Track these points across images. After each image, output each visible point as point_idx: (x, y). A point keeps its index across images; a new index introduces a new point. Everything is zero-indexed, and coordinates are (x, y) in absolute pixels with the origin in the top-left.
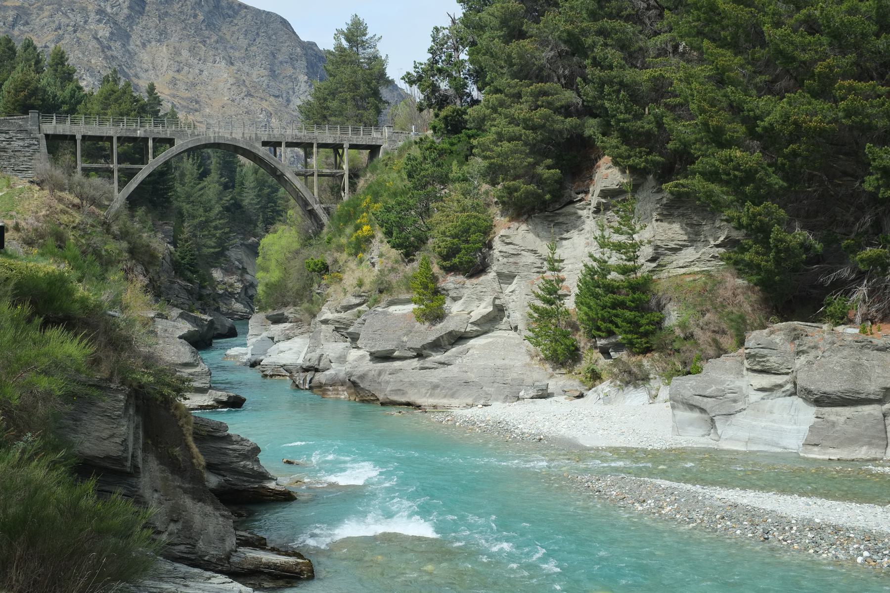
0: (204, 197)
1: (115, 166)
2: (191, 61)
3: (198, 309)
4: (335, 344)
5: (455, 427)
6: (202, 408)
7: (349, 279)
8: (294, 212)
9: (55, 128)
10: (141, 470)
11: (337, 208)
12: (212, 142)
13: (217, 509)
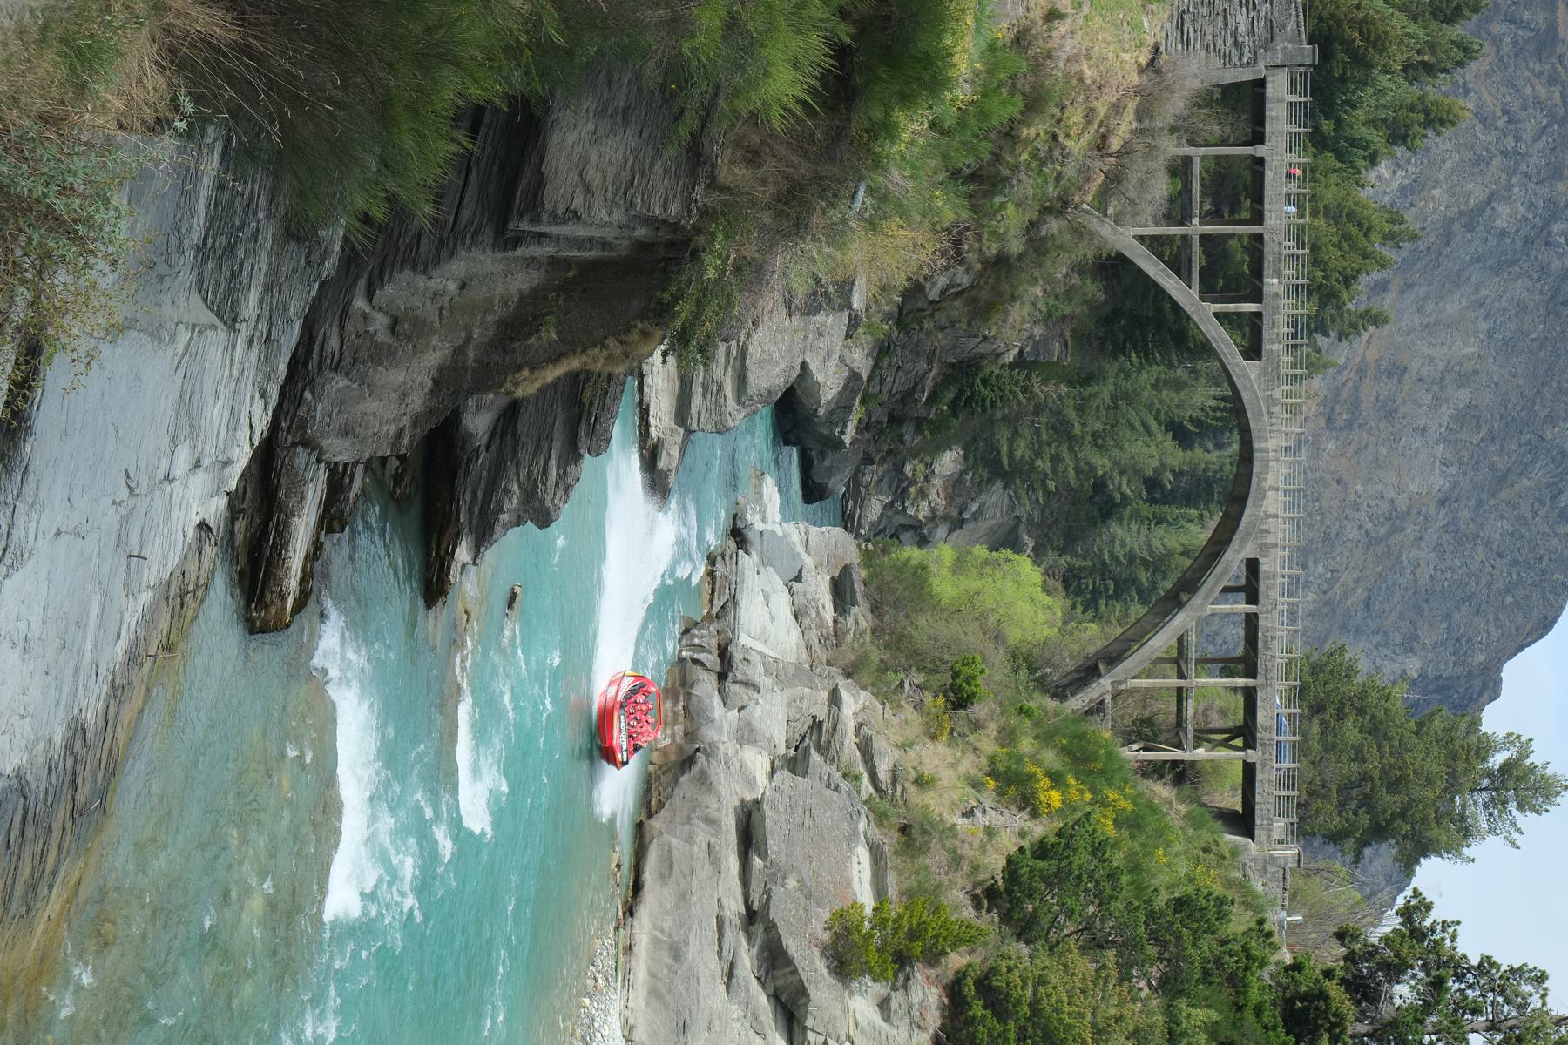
0: (1128, 433)
1: (1196, 228)
2: (1444, 408)
3: (869, 414)
4: (782, 719)
5: (580, 995)
6: (644, 412)
7: (934, 757)
8: (1093, 636)
9: (1280, 100)
10: (510, 254)
11: (1104, 731)
12: (1256, 445)
13: (415, 423)
